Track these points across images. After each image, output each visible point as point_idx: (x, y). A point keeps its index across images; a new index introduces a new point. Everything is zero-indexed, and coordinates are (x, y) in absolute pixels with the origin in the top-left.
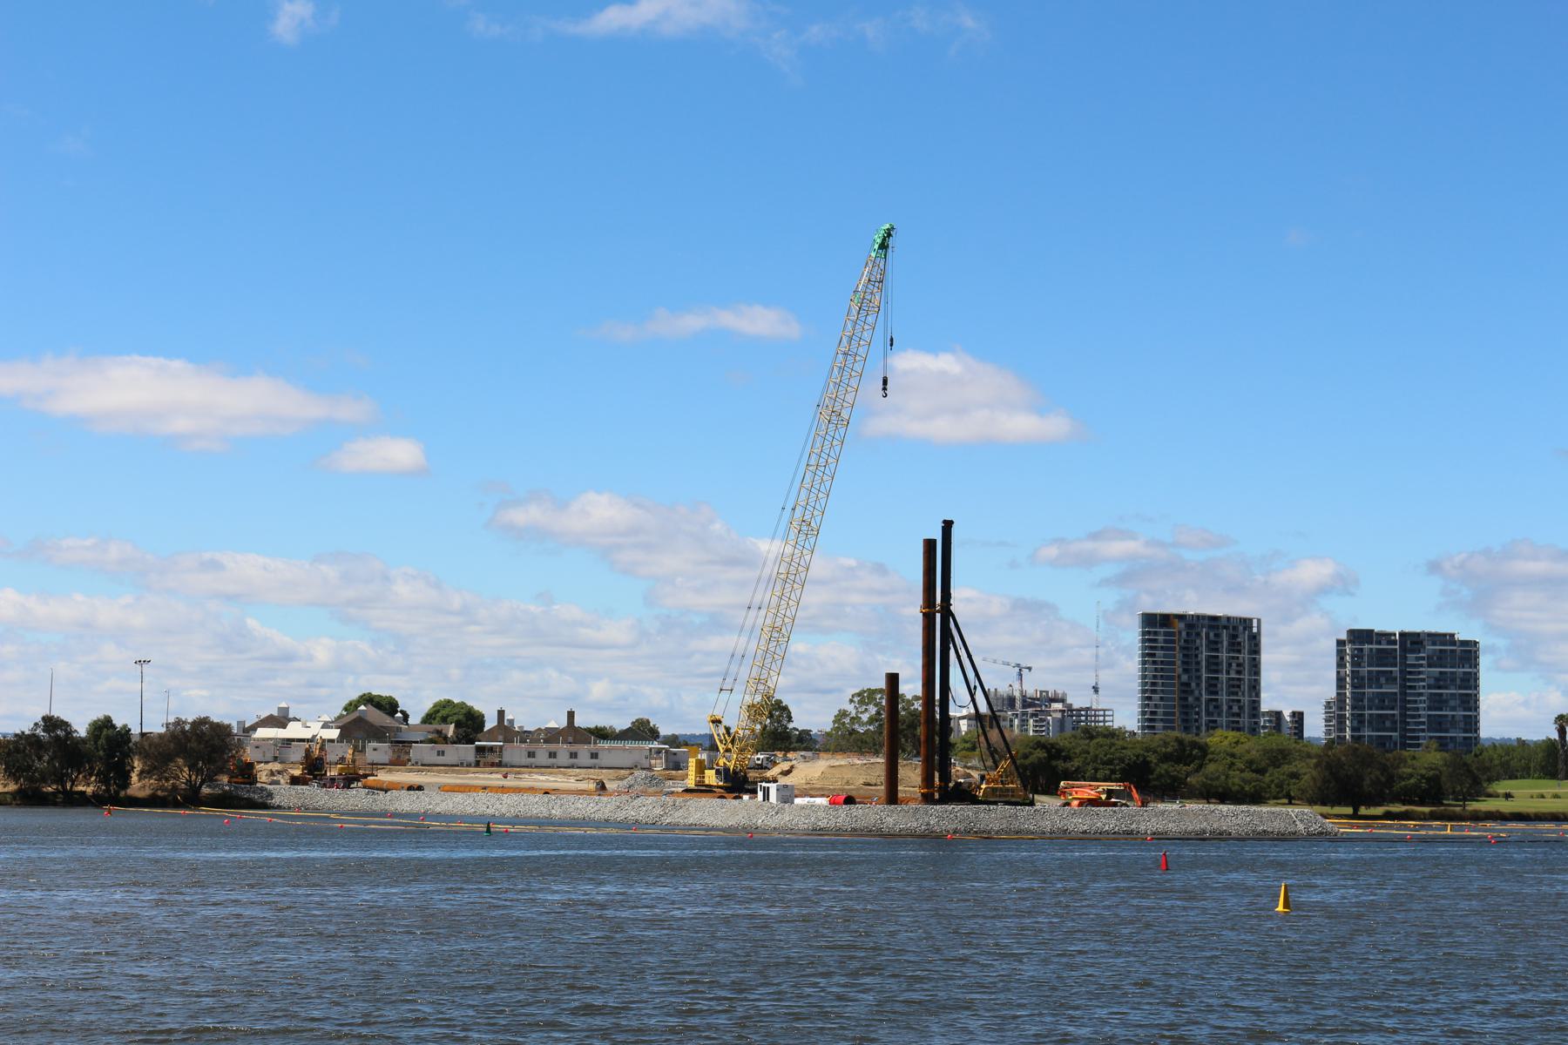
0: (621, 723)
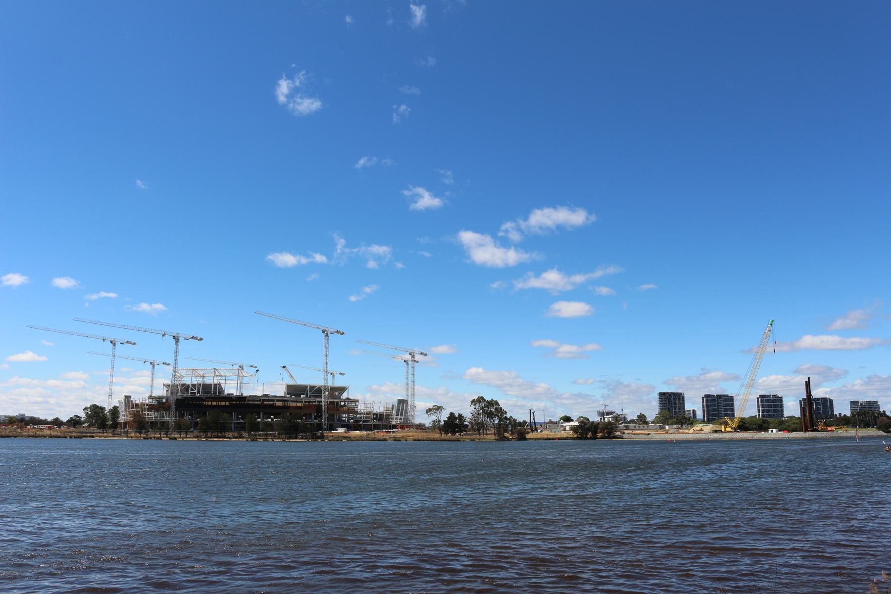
0: (50, 419)
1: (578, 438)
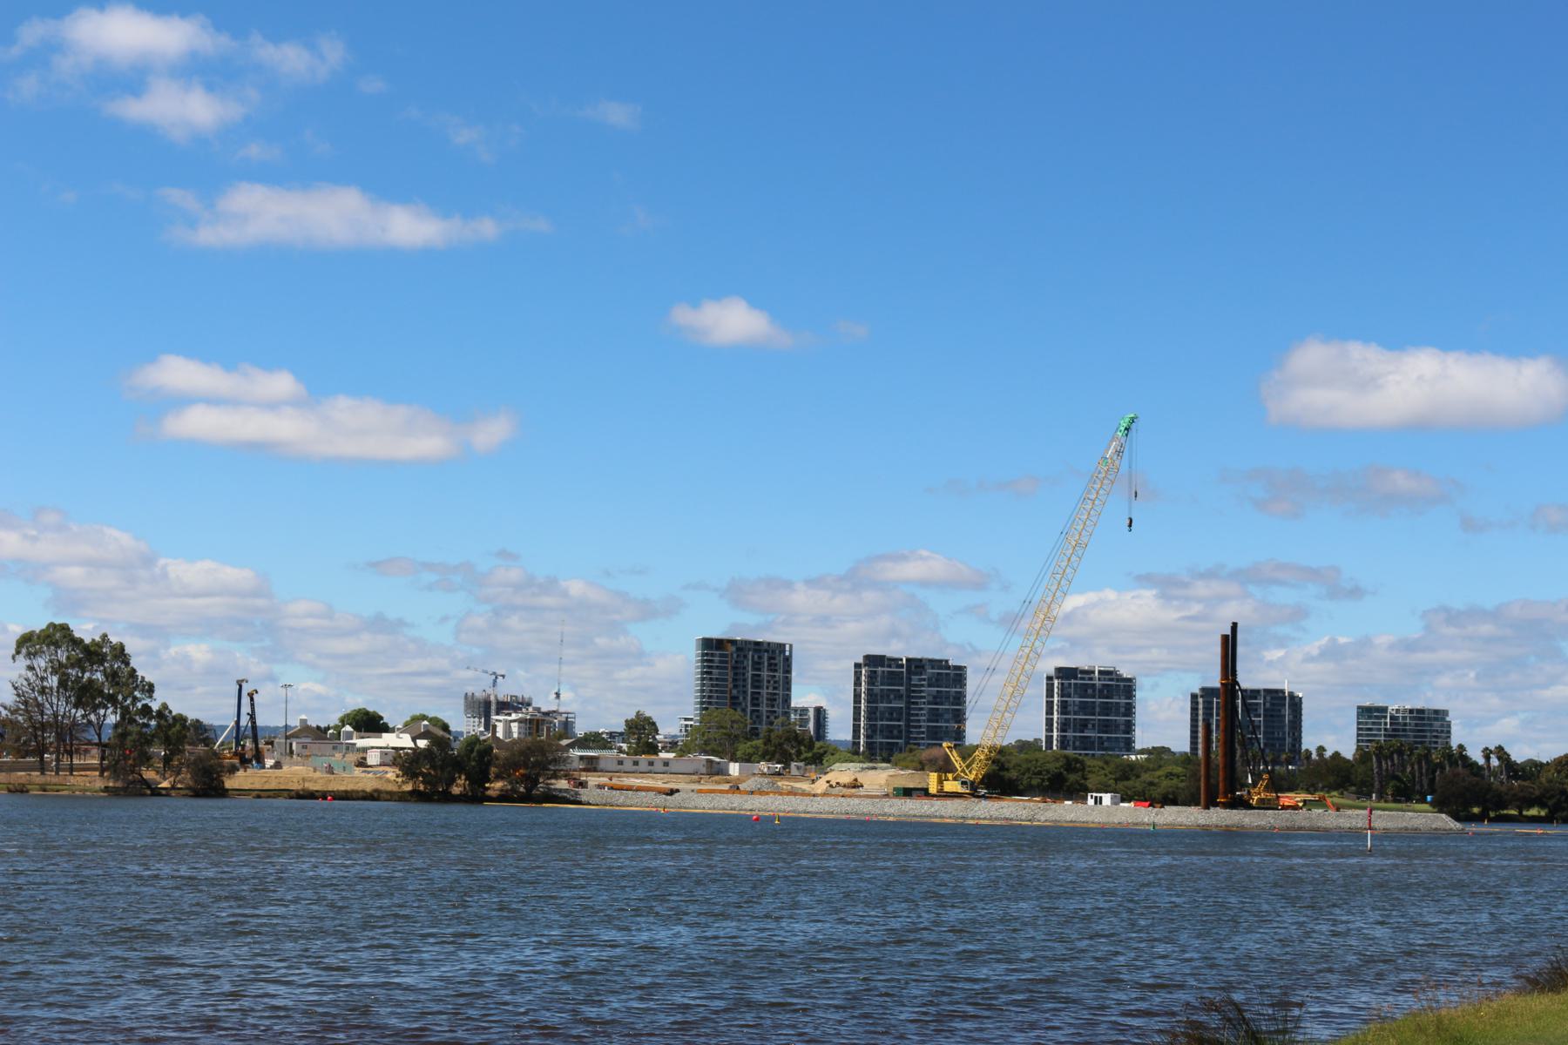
1: (417, 796)
